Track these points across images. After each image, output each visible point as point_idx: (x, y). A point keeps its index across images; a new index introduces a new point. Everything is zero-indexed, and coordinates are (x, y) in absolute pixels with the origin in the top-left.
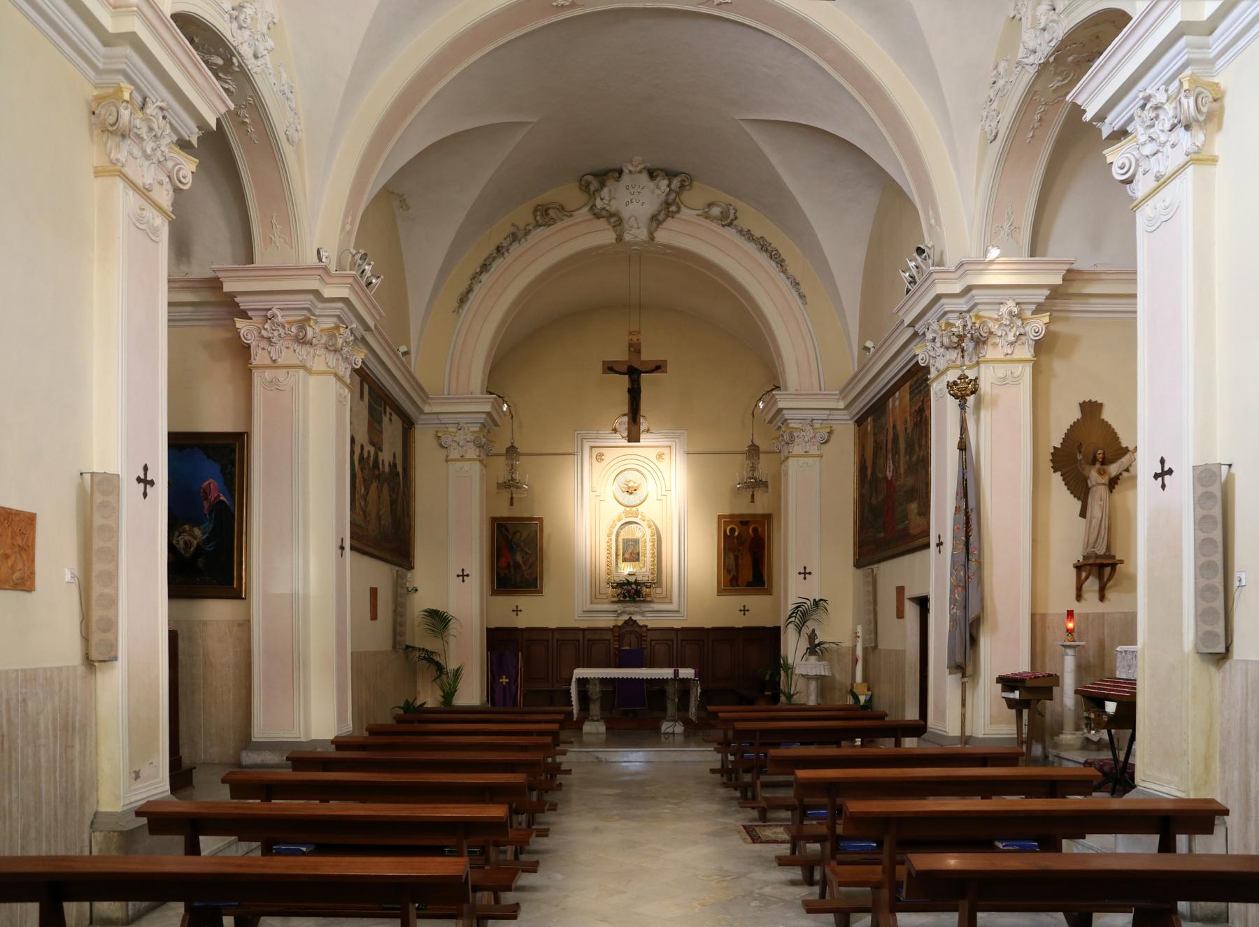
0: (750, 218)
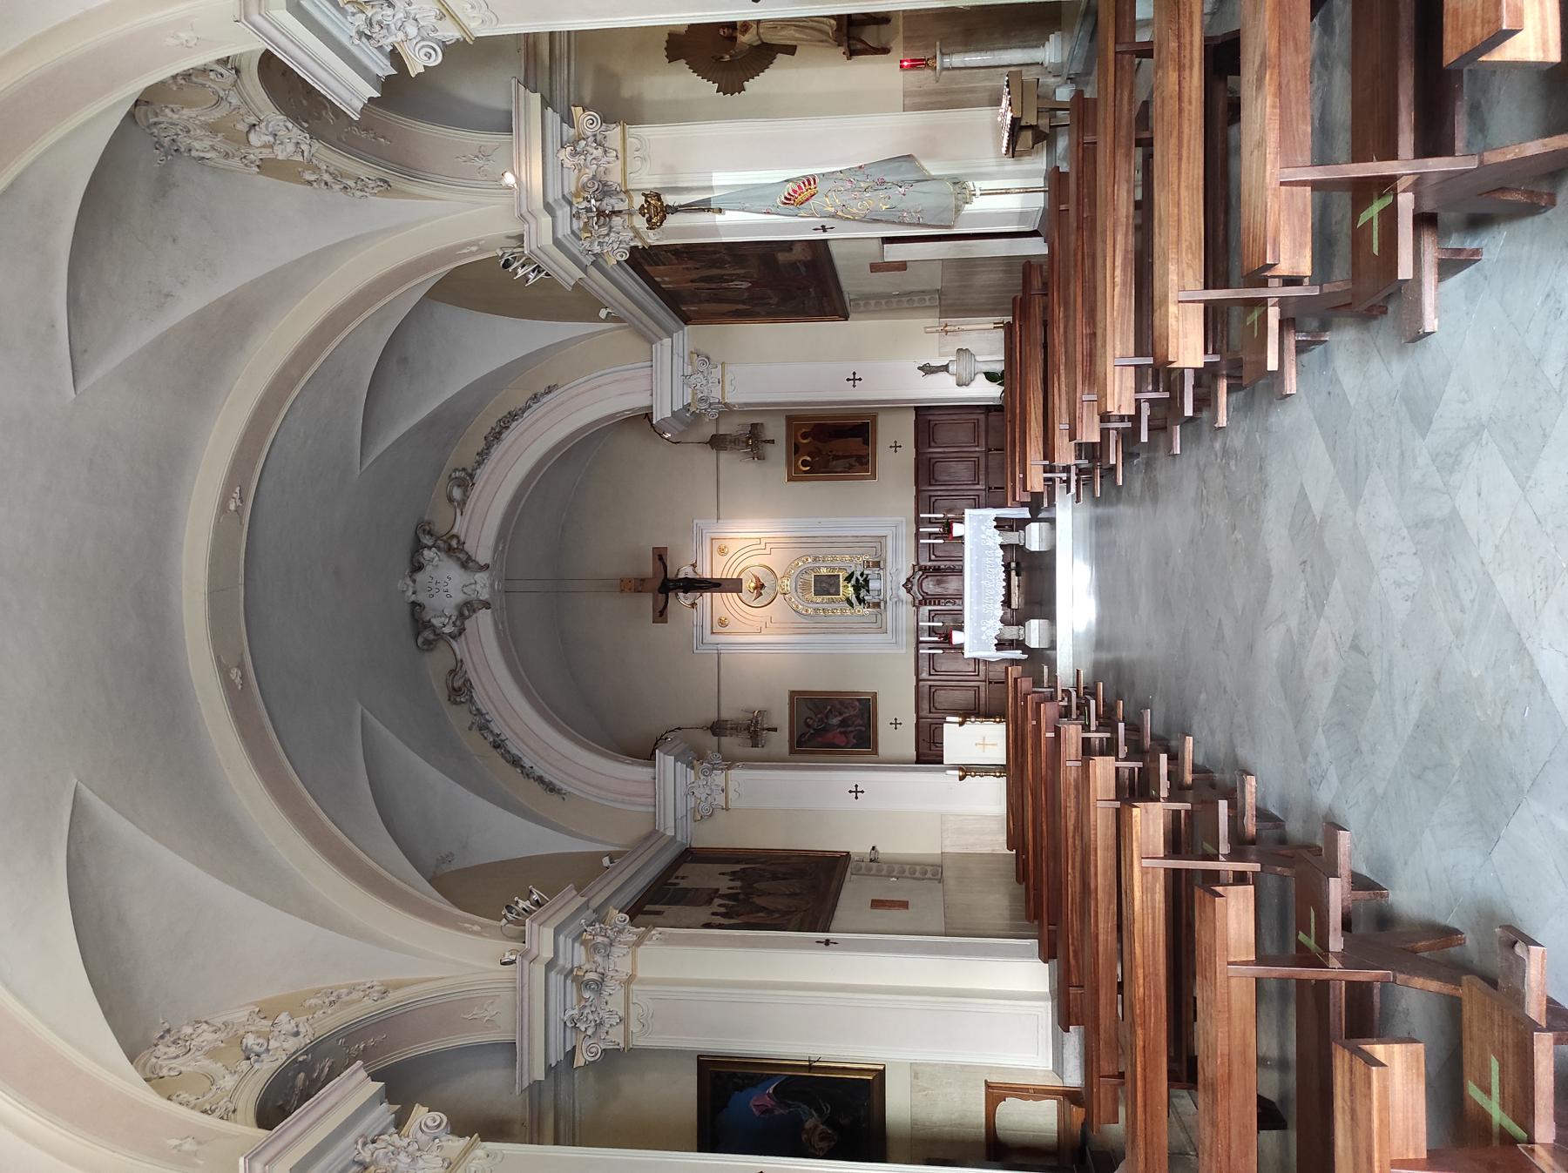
0: (462, 454)
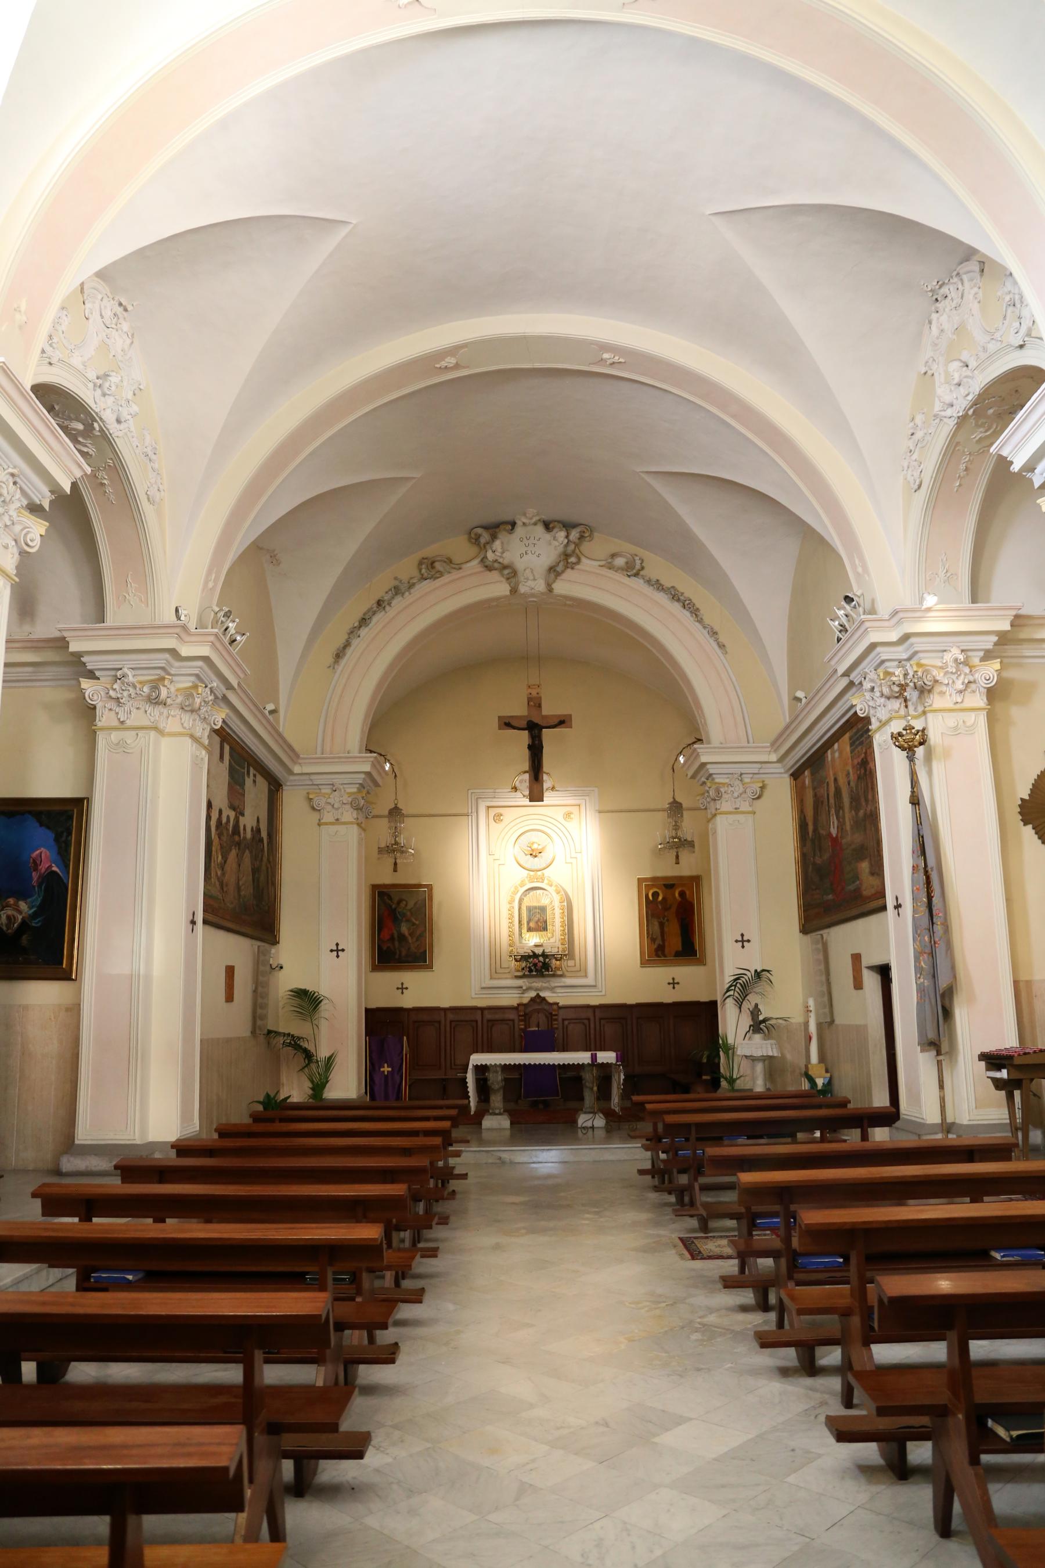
0: (657, 567)
